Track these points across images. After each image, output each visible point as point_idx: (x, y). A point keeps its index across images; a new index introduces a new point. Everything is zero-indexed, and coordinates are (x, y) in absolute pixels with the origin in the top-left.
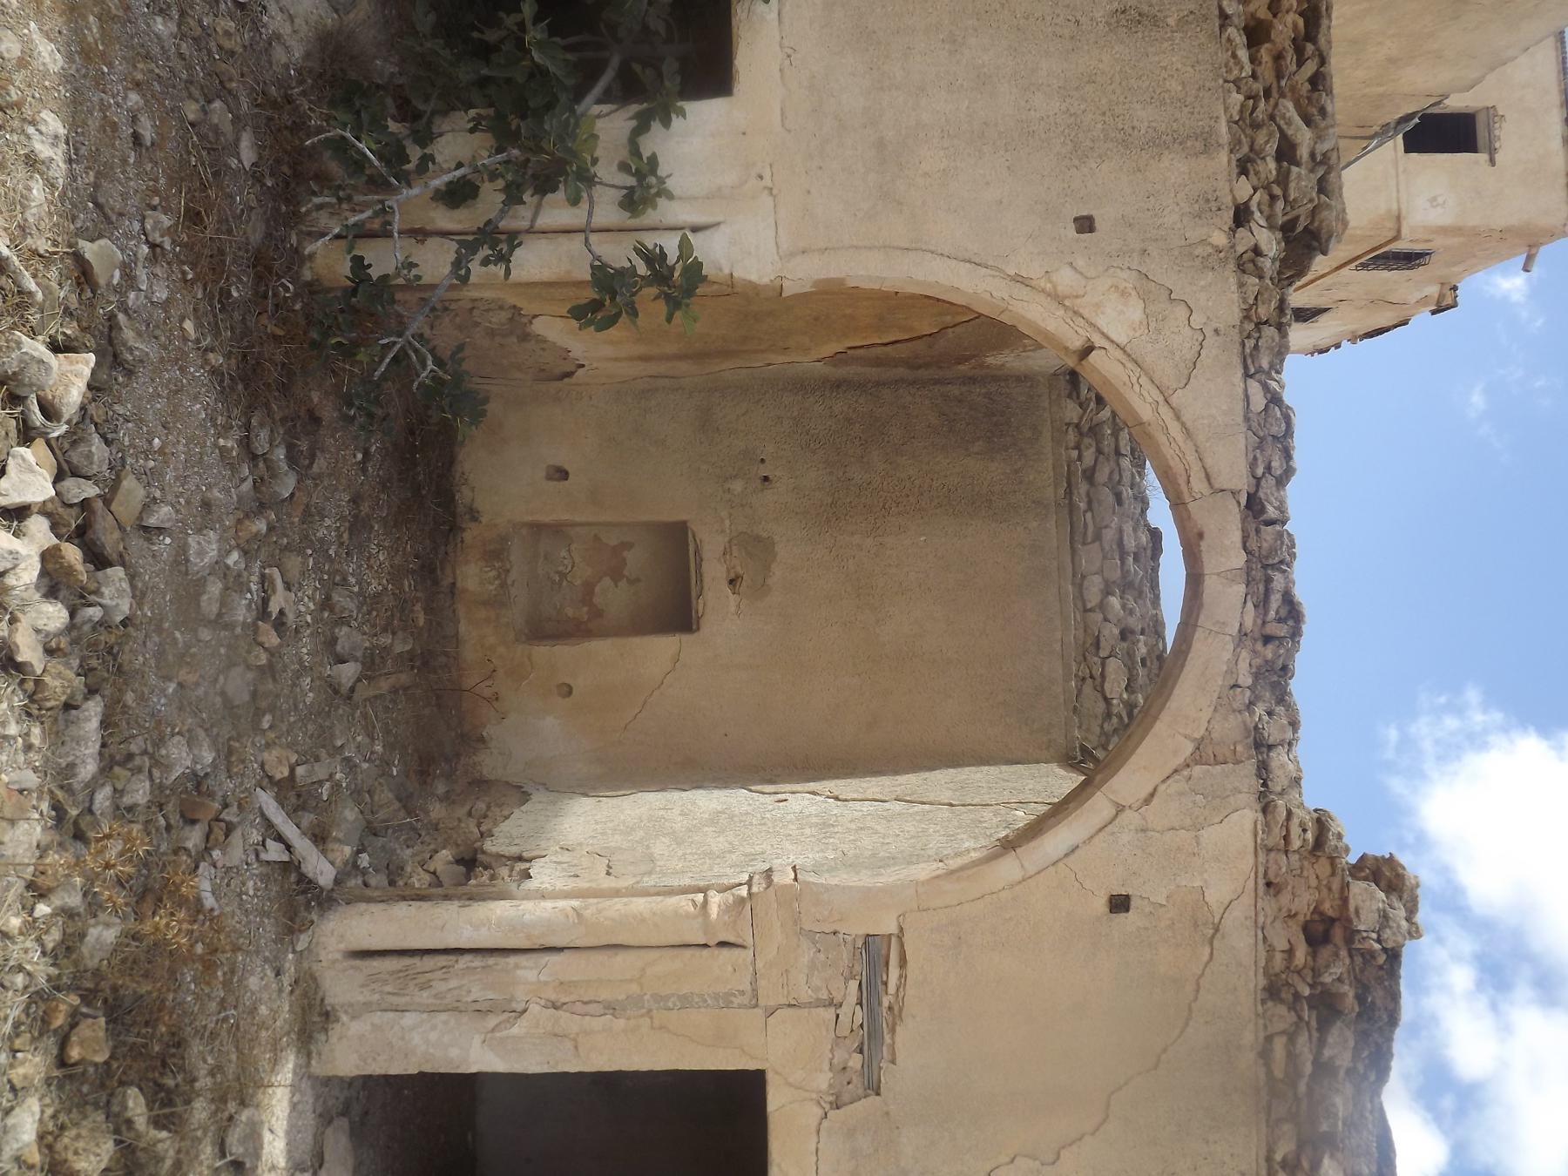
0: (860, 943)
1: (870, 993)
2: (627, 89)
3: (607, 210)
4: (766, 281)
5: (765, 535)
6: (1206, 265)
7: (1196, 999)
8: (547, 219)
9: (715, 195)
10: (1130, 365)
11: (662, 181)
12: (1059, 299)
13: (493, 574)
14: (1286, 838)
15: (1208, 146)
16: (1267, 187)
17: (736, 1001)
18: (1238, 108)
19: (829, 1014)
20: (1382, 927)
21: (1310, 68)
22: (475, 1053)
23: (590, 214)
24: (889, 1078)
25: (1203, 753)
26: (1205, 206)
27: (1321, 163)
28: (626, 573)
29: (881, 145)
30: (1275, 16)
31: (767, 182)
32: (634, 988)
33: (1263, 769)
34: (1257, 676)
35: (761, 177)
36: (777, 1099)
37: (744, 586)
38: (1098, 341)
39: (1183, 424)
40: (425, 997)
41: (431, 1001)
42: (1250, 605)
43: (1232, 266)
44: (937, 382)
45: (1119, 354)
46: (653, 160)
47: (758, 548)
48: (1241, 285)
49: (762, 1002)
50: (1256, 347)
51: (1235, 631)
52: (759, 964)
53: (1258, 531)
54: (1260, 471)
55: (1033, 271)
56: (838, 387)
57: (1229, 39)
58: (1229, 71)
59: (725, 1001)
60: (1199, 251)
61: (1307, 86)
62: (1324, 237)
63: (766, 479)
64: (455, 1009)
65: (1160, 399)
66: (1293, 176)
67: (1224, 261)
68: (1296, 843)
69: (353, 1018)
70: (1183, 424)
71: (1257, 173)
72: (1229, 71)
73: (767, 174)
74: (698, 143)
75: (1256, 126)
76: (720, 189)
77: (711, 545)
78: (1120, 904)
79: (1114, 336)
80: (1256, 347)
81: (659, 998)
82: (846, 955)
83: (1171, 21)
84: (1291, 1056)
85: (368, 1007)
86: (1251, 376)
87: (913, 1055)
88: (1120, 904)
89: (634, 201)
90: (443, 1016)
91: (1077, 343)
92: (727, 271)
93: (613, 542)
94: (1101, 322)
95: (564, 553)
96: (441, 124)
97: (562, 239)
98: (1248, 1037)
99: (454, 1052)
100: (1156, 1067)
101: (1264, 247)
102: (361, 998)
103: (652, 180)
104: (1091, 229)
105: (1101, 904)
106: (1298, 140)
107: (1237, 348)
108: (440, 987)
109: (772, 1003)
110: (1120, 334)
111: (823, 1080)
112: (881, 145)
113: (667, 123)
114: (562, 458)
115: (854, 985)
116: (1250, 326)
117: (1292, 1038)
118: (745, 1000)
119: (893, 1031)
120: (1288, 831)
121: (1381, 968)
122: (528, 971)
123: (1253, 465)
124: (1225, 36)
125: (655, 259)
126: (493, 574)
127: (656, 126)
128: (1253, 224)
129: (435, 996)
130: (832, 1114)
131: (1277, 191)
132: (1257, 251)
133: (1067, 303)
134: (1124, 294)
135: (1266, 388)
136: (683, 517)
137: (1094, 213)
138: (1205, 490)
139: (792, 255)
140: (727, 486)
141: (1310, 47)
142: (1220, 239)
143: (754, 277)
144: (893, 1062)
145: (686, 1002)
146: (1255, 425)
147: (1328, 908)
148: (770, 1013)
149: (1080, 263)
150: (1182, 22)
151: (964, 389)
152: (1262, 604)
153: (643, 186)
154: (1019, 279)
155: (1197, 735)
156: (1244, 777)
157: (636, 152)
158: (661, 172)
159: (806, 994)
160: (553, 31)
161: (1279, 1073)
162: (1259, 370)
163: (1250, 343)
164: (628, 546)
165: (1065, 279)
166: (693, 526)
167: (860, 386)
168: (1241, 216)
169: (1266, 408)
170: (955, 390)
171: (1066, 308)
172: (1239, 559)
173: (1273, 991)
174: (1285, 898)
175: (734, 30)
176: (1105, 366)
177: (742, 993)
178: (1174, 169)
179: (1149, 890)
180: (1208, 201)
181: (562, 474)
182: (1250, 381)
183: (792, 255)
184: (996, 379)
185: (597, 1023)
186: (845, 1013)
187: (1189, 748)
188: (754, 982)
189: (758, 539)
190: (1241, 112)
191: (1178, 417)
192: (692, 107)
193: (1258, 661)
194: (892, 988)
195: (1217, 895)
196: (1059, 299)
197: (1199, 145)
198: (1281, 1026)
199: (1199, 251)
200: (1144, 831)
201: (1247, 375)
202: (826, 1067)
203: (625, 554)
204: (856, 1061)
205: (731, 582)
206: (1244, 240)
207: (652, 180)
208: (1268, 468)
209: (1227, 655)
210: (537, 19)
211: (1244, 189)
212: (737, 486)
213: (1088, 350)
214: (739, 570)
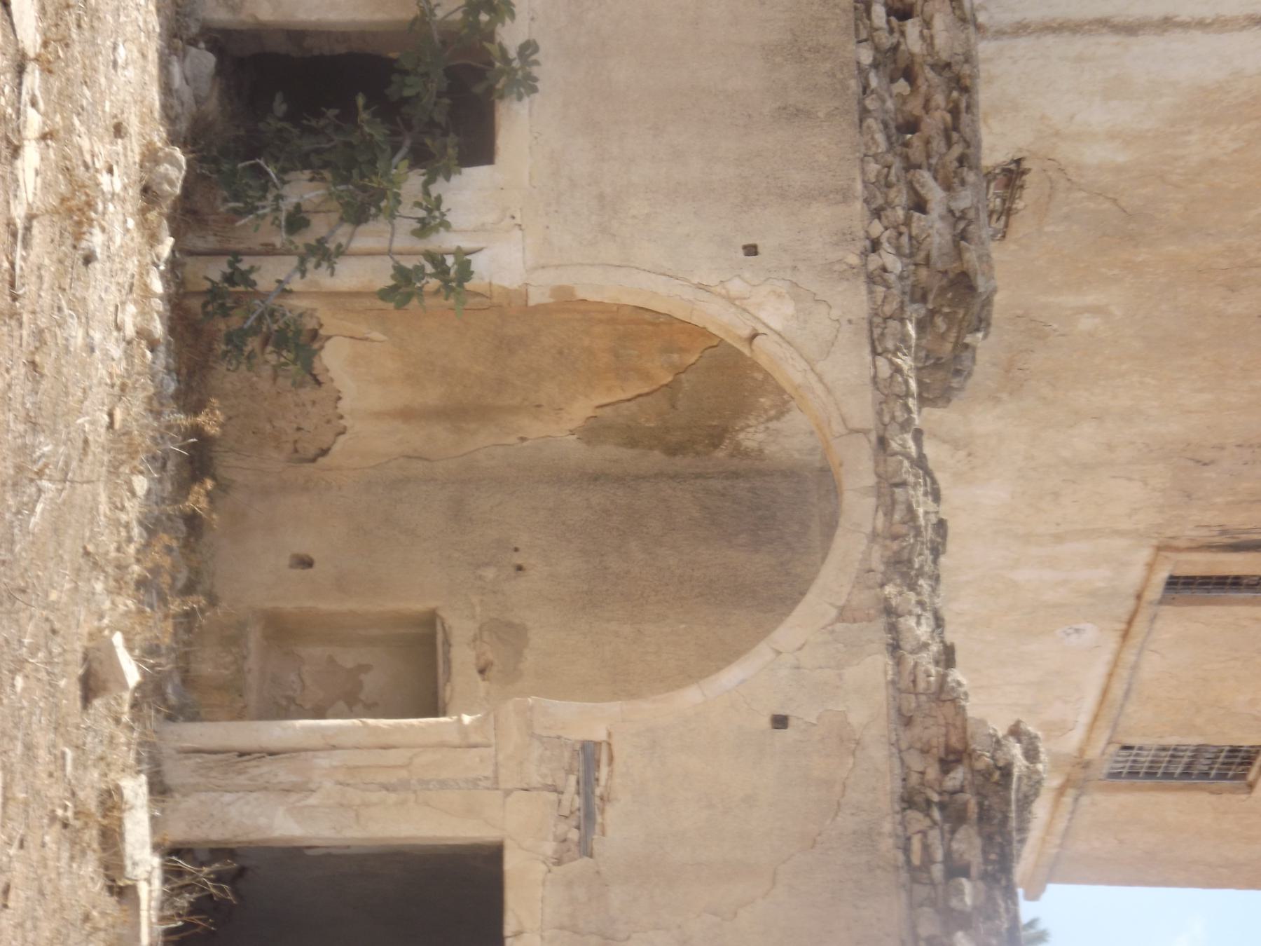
0: (578, 747)
1: (587, 785)
2: (421, 158)
3: (405, 226)
4: (515, 286)
5: (517, 621)
6: (842, 276)
7: (843, 796)
8: (359, 243)
9: (481, 229)
10: (785, 345)
11: (443, 215)
12: (731, 300)
13: (229, 659)
14: (914, 682)
15: (846, 196)
16: (896, 228)
17: (482, 784)
18: (874, 173)
19: (553, 796)
20: (996, 750)
21: (957, 150)
22: (280, 823)
23: (391, 241)
24: (597, 844)
25: (844, 614)
26: (845, 237)
27: (961, 218)
28: (362, 697)
29: (601, 197)
30: (927, 113)
31: (518, 221)
32: (403, 774)
33: (893, 628)
34: (887, 564)
35: (513, 217)
36: (511, 862)
37: (492, 673)
38: (761, 329)
39: (825, 385)
40: (242, 780)
41: (246, 782)
42: (880, 514)
43: (863, 278)
44: (698, 476)
45: (776, 338)
46: (439, 200)
47: (508, 634)
48: (871, 292)
49: (502, 786)
50: (882, 334)
51: (868, 529)
52: (501, 757)
53: (885, 461)
54: (887, 419)
55: (712, 280)
56: (596, 479)
57: (869, 127)
58: (868, 148)
59: (475, 783)
60: (837, 267)
61: (956, 164)
62: (971, 274)
63: (520, 568)
64: (266, 789)
65: (808, 368)
66: (915, 219)
67: (858, 275)
68: (922, 685)
69: (185, 795)
70: (825, 385)
71: (887, 217)
72: (868, 148)
73: (518, 215)
74: (468, 194)
75: (889, 185)
76: (483, 225)
77: (461, 630)
78: (780, 722)
79: (772, 325)
80: (882, 334)
81: (424, 783)
82: (567, 754)
83: (821, 115)
84: (926, 847)
85: (196, 789)
86: (879, 354)
87: (619, 829)
88: (780, 722)
89: (424, 228)
90: (255, 795)
91: (746, 332)
92: (487, 281)
93: (350, 665)
94: (763, 315)
95: (293, 677)
96: (292, 175)
97: (369, 258)
98: (887, 827)
99: (262, 821)
100: (813, 847)
101: (889, 266)
102: (192, 781)
103: (437, 214)
104: (756, 253)
105: (765, 722)
106: (929, 196)
107: (865, 333)
108: (256, 772)
109: (509, 786)
110: (776, 324)
111: (549, 847)
112: (601, 197)
113: (448, 179)
114: (305, 544)
115: (573, 779)
116: (877, 320)
117: (924, 833)
118: (488, 784)
119: (602, 811)
120: (915, 677)
121: (997, 783)
122: (323, 761)
123: (880, 414)
124: (865, 125)
125: (436, 259)
126: (229, 659)
127: (441, 179)
128: (882, 252)
129: (250, 779)
130: (555, 869)
131: (903, 229)
132: (884, 270)
133: (737, 302)
134: (779, 296)
135: (891, 363)
136: (432, 604)
137: (758, 243)
138: (842, 430)
139: (535, 269)
140: (480, 572)
141: (955, 136)
142: (854, 259)
143: (506, 284)
144: (603, 834)
145: (443, 784)
146: (881, 386)
147: (954, 741)
148: (508, 793)
149: (747, 275)
150: (830, 115)
151: (727, 483)
152: (889, 513)
153: (431, 219)
154: (700, 287)
155: (841, 602)
156: (877, 632)
157: (427, 193)
158: (443, 208)
159: (536, 780)
160: (375, 115)
161: (916, 860)
162: (886, 351)
163: (877, 332)
164: (364, 668)
165: (736, 287)
166: (442, 613)
167: (620, 480)
168: (875, 245)
169: (892, 377)
170: (717, 484)
171: (737, 307)
172: (871, 480)
173: (909, 801)
174: (917, 730)
175: (497, 128)
176: (767, 351)
177: (486, 778)
178: (821, 213)
179: (803, 712)
180: (844, 234)
181: (305, 562)
182: (878, 358)
183: (535, 269)
184: (760, 473)
185: (374, 797)
186: (566, 798)
187: (833, 613)
188: (496, 772)
189: (510, 625)
190: (877, 176)
191: (821, 380)
192: (466, 171)
193: (888, 553)
194: (602, 782)
195: (857, 718)
196: (731, 300)
197: (839, 197)
198: (918, 827)
199: (837, 267)
200: (798, 668)
201: (875, 353)
202: (551, 837)
203: (363, 677)
204: (574, 835)
205: (482, 671)
206: (874, 262)
207: (437, 214)
208: (893, 418)
209: (862, 548)
210: (366, 107)
211: (876, 228)
212: (490, 573)
213: (754, 336)
214: (490, 656)
